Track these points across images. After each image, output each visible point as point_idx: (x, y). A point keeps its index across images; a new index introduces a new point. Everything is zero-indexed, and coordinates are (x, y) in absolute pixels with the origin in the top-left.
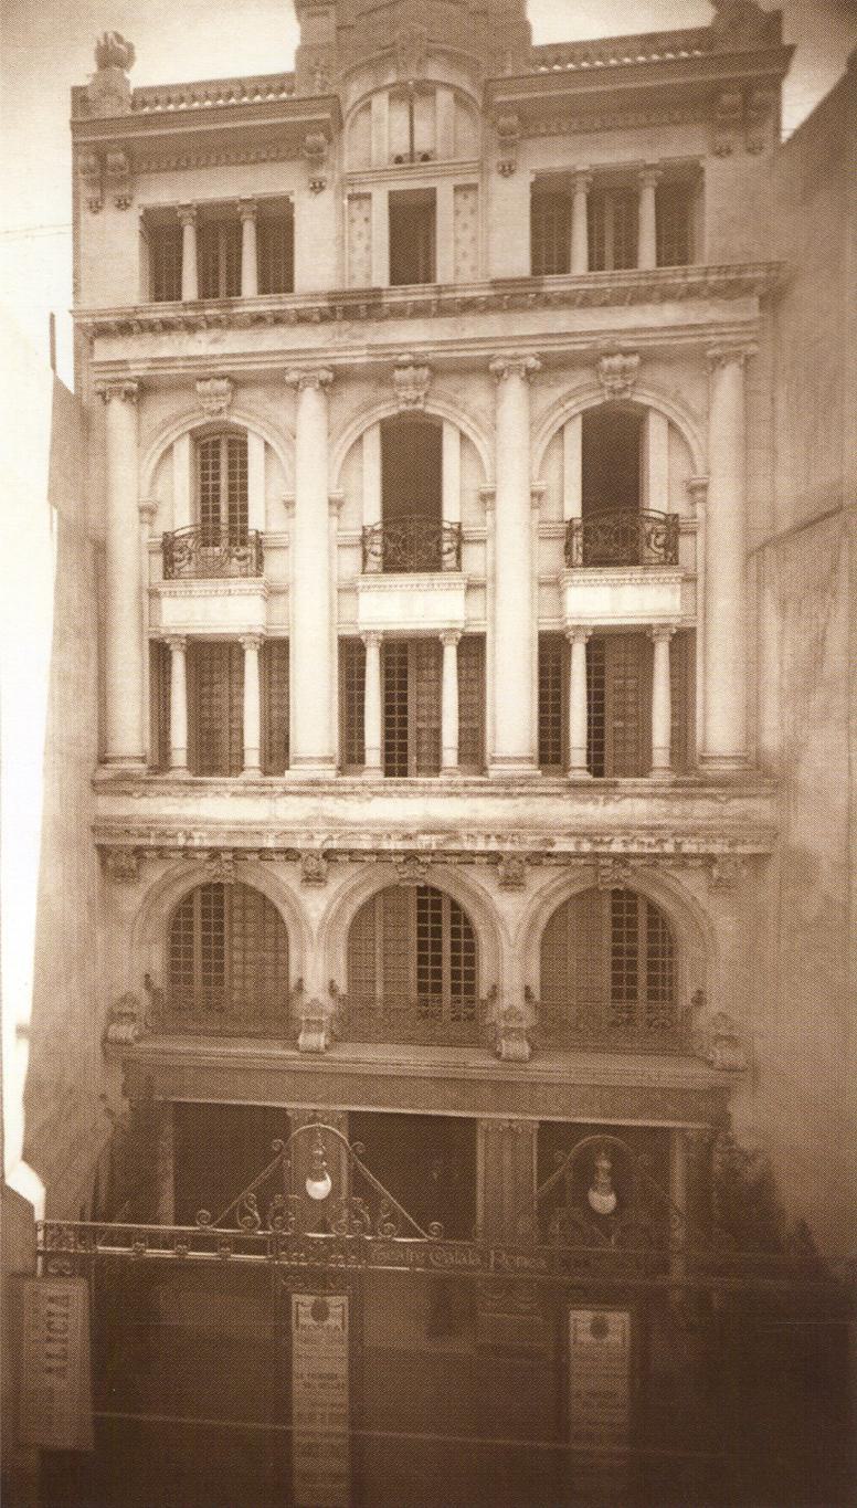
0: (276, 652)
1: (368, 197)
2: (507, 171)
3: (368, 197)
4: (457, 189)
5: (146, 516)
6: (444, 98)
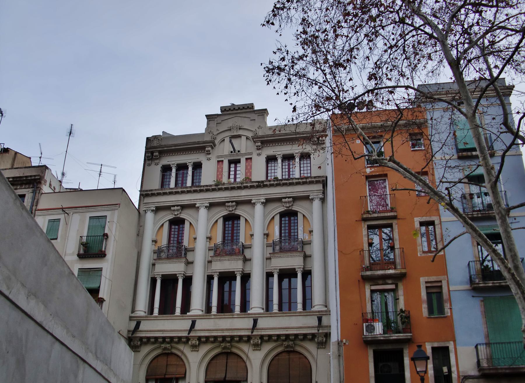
0: (188, 281)
1: (222, 161)
2: (259, 155)
3: (222, 161)
4: (247, 159)
5: (154, 243)
6: (244, 138)
